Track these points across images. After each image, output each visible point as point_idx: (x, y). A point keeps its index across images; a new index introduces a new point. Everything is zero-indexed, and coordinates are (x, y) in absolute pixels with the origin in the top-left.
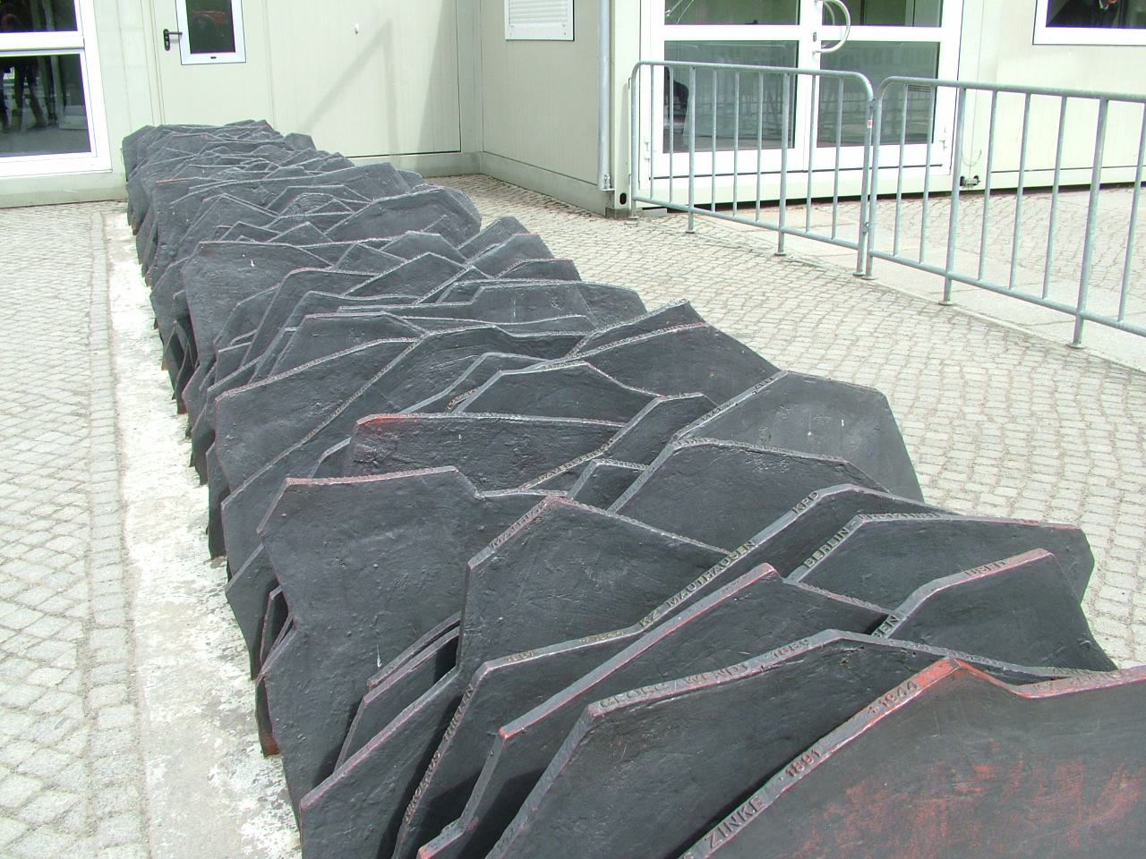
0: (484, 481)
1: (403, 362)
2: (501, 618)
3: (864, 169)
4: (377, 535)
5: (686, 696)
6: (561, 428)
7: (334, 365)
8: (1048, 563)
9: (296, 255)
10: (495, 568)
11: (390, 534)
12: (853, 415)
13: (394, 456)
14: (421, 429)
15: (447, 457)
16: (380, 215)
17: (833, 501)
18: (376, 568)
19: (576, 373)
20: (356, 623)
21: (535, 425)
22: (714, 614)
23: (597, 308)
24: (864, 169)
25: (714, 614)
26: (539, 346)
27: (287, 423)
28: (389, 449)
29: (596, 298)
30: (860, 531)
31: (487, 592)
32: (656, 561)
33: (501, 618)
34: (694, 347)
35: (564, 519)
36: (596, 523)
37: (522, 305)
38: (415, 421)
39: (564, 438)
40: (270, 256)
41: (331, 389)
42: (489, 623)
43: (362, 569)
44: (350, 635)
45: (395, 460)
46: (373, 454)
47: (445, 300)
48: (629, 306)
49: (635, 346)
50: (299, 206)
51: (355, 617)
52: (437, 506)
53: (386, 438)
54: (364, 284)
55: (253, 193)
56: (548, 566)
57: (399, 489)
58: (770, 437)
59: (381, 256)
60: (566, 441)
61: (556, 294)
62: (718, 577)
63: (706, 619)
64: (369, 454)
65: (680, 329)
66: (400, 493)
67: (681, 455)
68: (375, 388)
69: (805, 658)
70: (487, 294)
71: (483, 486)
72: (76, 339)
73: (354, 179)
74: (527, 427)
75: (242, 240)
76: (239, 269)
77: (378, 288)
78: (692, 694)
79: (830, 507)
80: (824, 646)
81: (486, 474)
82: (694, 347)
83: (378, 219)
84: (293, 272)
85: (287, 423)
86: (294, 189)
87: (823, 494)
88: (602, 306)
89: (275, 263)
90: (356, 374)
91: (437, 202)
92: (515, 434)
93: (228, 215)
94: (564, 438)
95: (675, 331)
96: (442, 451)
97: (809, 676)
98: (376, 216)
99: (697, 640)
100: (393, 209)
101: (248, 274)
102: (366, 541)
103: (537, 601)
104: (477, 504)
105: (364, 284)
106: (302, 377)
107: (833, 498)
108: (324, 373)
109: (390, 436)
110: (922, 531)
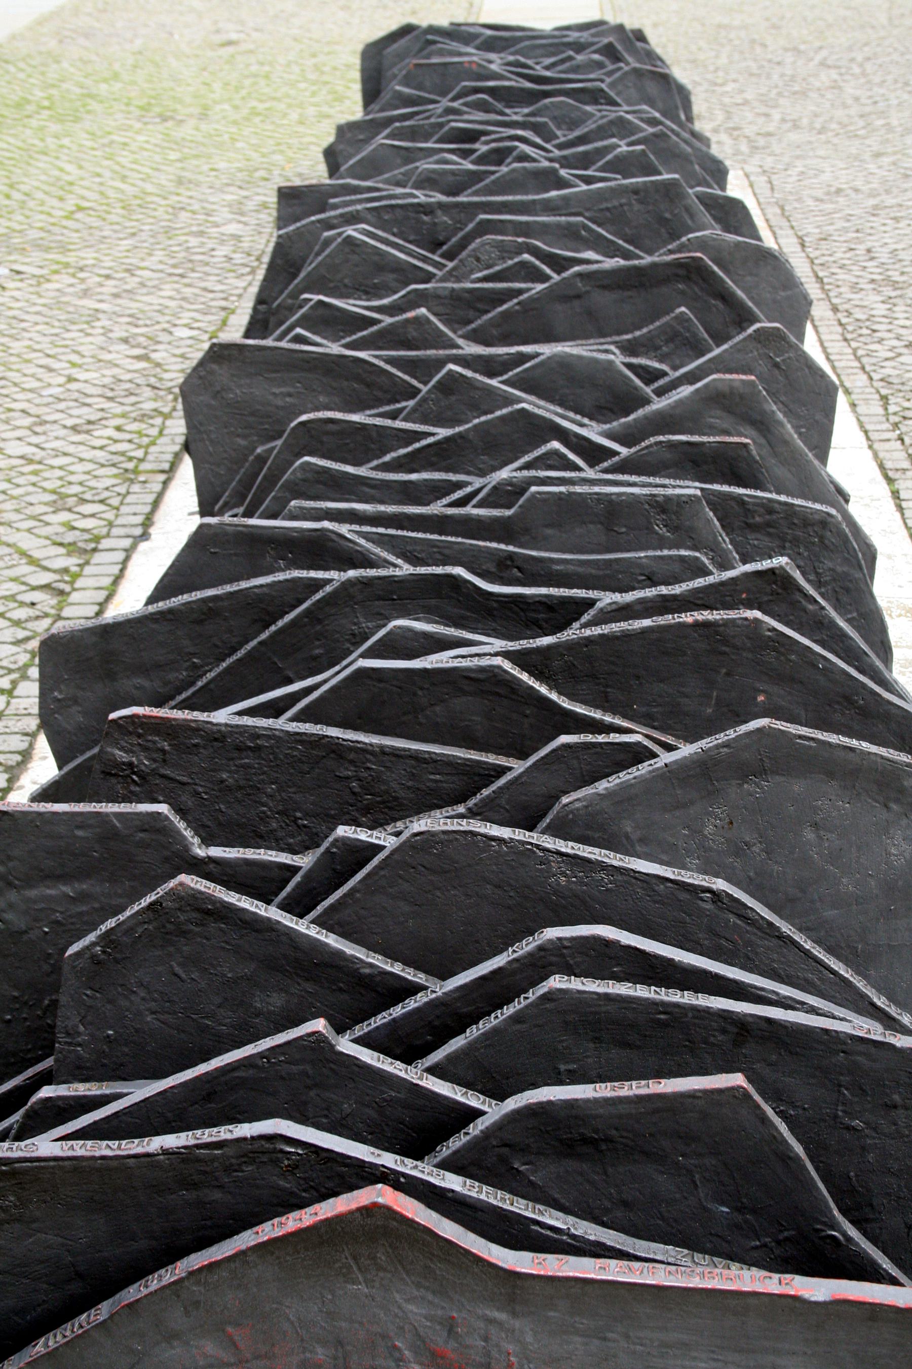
0: (305, 826)
1: (308, 612)
2: (111, 1032)
3: (888, 414)
4: (48, 887)
5: (52, 1163)
6: (425, 761)
7: (221, 603)
8: (735, 1097)
9: (370, 372)
10: (96, 961)
11: (67, 890)
12: (894, 806)
13: (162, 771)
14: (202, 737)
15: (242, 783)
16: (578, 297)
17: (566, 947)
18: (46, 933)
19: (481, 676)
20: (17, 1006)
21: (383, 751)
22: (236, 1074)
23: (759, 536)
24: (888, 414)
25: (236, 1074)
26: (534, 611)
27: (146, 684)
28: (155, 760)
29: (758, 519)
30: (547, 997)
31: (88, 992)
32: (341, 990)
33: (111, 1032)
34: (726, 649)
35: (198, 910)
36: (245, 922)
37: (601, 523)
38: (193, 725)
39: (432, 777)
40: (328, 372)
41: (215, 640)
42: (92, 1035)
43: (26, 932)
44: (9, 1021)
45: (163, 776)
46: (130, 765)
47: (479, 505)
48: (822, 538)
49: (617, 638)
50: (478, 260)
51: (16, 998)
52: (139, 859)
53: (150, 745)
54: (410, 449)
55: (424, 223)
56: (178, 970)
57: (78, 827)
58: (731, 823)
59: (490, 391)
60: (436, 781)
61: (664, 511)
62: (377, 1028)
63: (223, 1079)
64: (124, 763)
65: (700, 618)
66: (80, 833)
67: (422, 841)
68: (263, 649)
69: (225, 1149)
70: (539, 500)
71: (207, 841)
72: (46, 474)
73: (609, 205)
74: (372, 753)
75: (299, 339)
76: (277, 391)
77: (434, 459)
78: (61, 1163)
79: (562, 956)
80: (252, 1138)
81: (307, 815)
82: (726, 649)
83: (576, 303)
84: (304, 418)
85: (146, 684)
86: (489, 221)
87: (552, 933)
88: (769, 535)
89: (334, 384)
90: (255, 621)
91: (687, 279)
92: (352, 762)
93: (357, 266)
94: (432, 777)
95: (690, 620)
96: (237, 772)
97: (235, 1174)
98: (566, 298)
99: (213, 1105)
100: (604, 287)
101: (288, 399)
102: (33, 893)
103: (161, 1017)
104: (195, 864)
105: (410, 449)
106: (171, 617)
107: (566, 943)
108: (204, 614)
109: (154, 742)
110: (662, 1016)
